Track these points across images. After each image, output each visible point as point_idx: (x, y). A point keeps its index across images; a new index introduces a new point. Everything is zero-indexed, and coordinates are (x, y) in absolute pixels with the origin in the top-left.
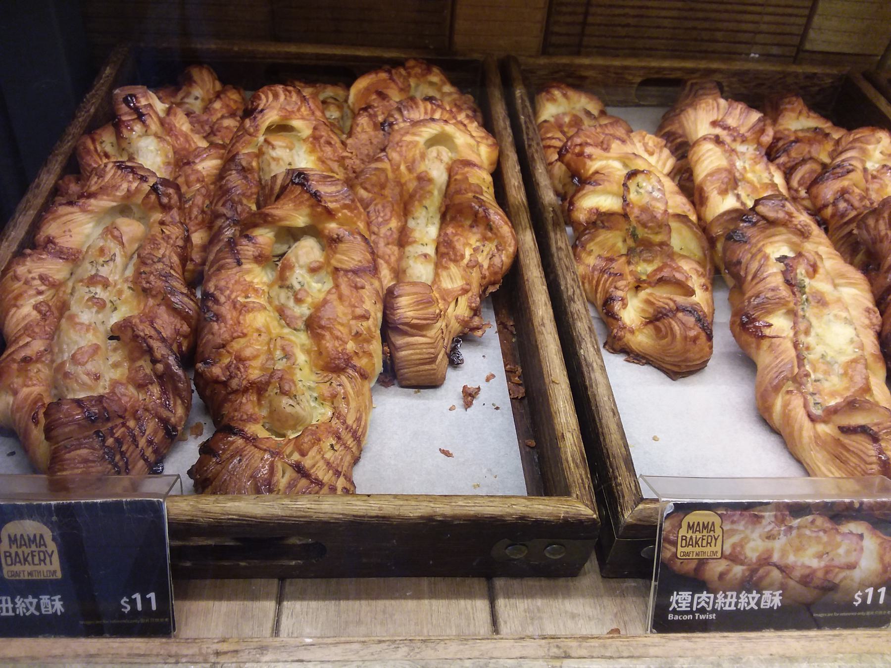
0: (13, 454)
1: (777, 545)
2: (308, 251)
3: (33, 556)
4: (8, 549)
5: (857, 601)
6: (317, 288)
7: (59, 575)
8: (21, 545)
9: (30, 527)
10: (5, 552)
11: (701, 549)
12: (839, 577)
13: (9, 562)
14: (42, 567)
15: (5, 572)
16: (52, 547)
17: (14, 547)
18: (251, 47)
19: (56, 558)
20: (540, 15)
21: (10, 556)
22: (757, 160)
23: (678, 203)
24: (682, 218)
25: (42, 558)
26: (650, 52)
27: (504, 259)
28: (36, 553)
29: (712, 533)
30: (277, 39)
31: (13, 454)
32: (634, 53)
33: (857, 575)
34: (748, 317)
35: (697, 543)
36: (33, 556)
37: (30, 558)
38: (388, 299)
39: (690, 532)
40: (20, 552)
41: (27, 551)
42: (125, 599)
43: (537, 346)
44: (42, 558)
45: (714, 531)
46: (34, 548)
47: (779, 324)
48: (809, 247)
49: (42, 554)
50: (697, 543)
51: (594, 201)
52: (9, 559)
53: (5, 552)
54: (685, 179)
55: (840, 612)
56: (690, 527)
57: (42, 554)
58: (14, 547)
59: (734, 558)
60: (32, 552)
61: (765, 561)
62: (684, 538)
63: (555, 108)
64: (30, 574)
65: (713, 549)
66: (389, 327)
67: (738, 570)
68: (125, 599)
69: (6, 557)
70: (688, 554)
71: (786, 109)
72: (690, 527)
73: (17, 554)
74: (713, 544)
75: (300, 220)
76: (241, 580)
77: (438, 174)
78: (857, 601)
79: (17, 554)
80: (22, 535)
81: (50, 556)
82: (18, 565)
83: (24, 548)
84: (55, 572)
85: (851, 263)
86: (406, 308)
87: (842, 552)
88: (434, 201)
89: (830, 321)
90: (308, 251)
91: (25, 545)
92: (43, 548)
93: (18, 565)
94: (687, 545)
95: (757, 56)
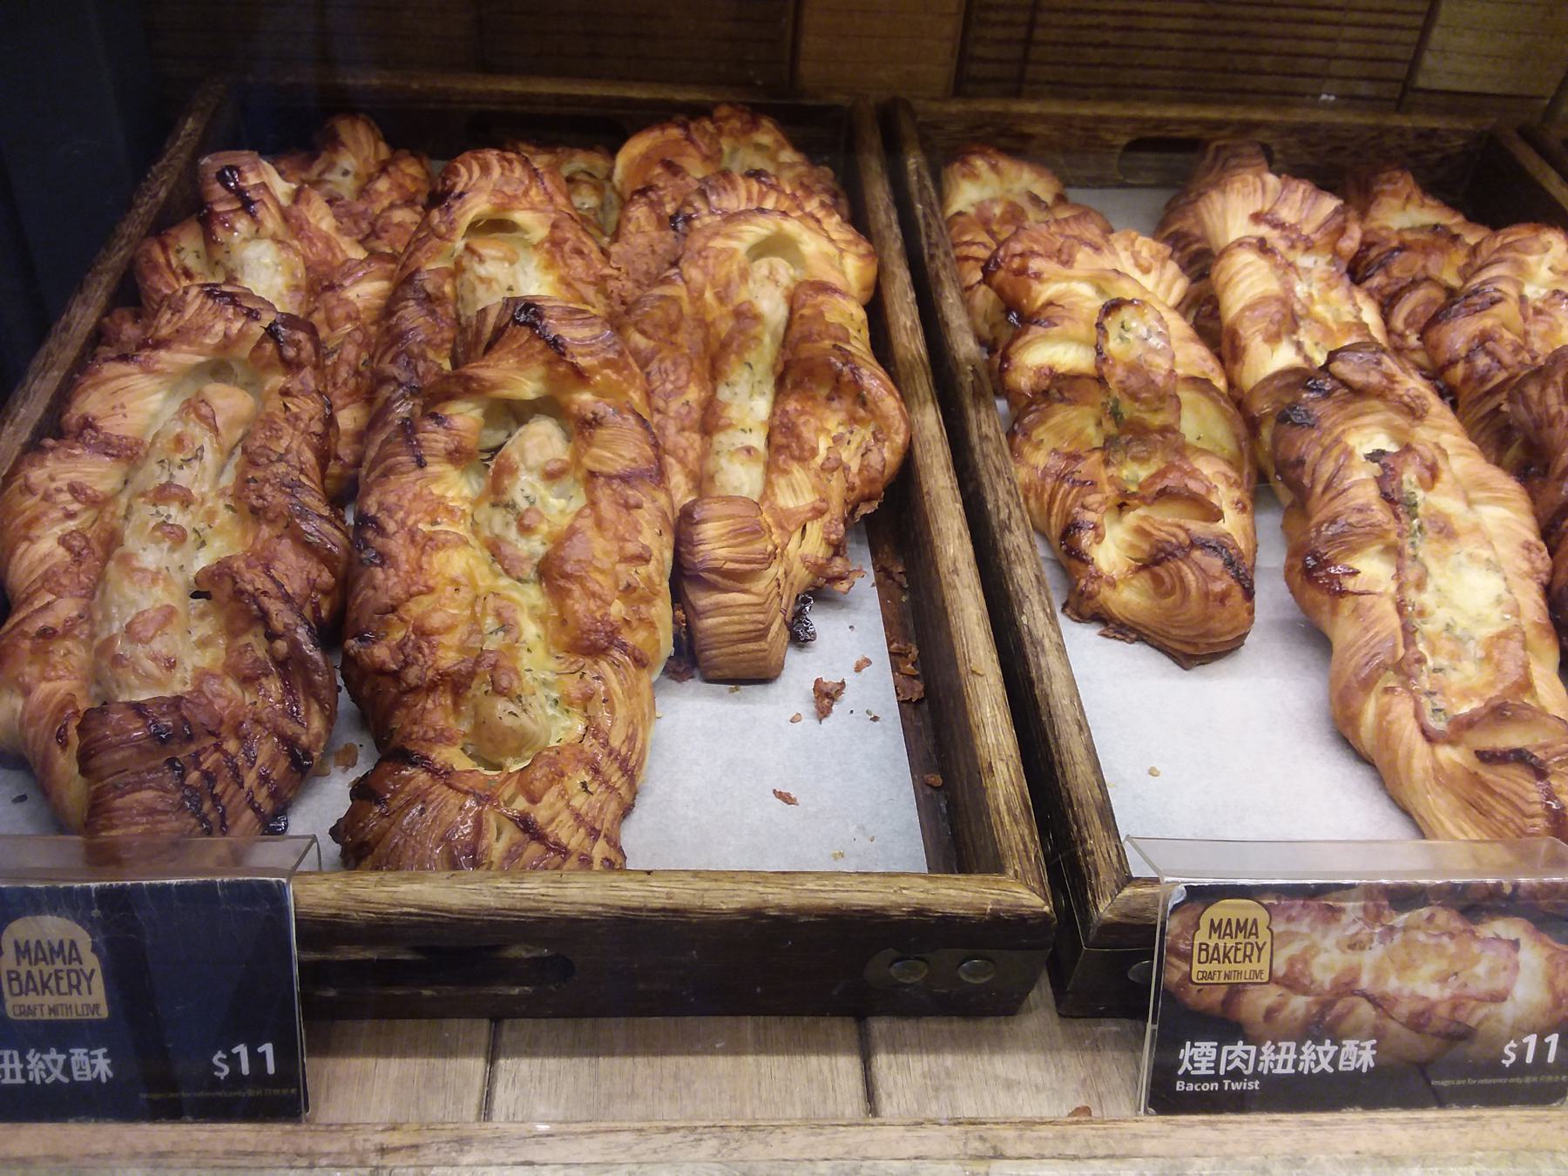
0: (22, 798)
1: (1368, 959)
2: (542, 441)
3: (58, 979)
4: (13, 966)
5: (1508, 1058)
6: (559, 506)
7: (104, 1012)
8: (37, 960)
9: (53, 927)
10: (9, 972)
11: (1234, 967)
12: (1477, 1015)
13: (16, 989)
14: (74, 999)
15: (9, 1006)
16: (91, 962)
17: (25, 962)
18: (441, 83)
19: (98, 982)
20: (950, 27)
21: (18, 978)
22: (1332, 282)
23: (1194, 358)
24: (1200, 384)
25: (74, 982)
26: (1144, 91)
27: (886, 456)
28: (63, 974)
29: (1253, 939)
30: (488, 68)
31: (22, 798)
32: (1116, 93)
33: (1508, 1012)
34: (1315, 559)
35: (1226, 956)
36: (58, 979)
37: (52, 983)
38: (683, 527)
39: (1215, 936)
40: (35, 971)
41: (48, 969)
42: (220, 1055)
43: (945, 610)
44: (74, 982)
45: (1256, 935)
46: (59, 964)
47: (1371, 570)
48: (1423, 435)
49: (73, 976)
50: (1226, 956)
51: (1045, 354)
52: (15, 984)
53: (9, 972)
54: (1205, 314)
55: (1478, 1078)
56: (1214, 928)
57: (73, 976)
58: (25, 962)
59: (1292, 982)
60: (57, 971)
61: (1347, 987)
62: (1204, 947)
63: (976, 190)
64: (53, 1010)
65: (1255, 966)
66: (685, 576)
67: (1299, 1004)
68: (220, 1055)
69: (10, 980)
70: (1211, 975)
71: (1383, 192)
72: (1214, 928)
73: (29, 975)
74: (1254, 958)
75: (528, 387)
76: (425, 1021)
77: (771, 307)
78: (1508, 1058)
79: (29, 975)
80: (38, 942)
81: (89, 979)
82: (32, 994)
83: (42, 965)
84: (96, 1006)
85: (1498, 464)
86: (715, 542)
87: (1482, 971)
88: (764, 353)
89: (1460, 564)
90: (542, 441)
91: (44, 959)
92: (75, 965)
93: (32, 994)
94: (1209, 960)
95: (1332, 98)
